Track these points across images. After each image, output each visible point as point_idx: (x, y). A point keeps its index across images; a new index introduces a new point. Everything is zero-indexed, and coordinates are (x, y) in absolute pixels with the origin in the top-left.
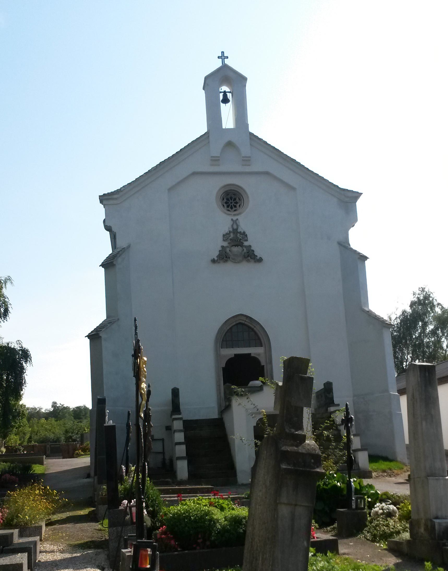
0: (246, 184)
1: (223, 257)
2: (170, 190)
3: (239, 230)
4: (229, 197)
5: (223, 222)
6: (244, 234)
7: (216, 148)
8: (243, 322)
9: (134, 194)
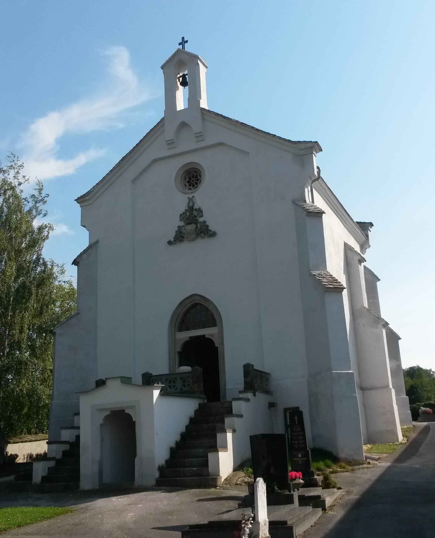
0: (202, 160)
1: (179, 237)
2: (134, 181)
4: (191, 175)
5: (180, 202)
6: (200, 211)
7: (170, 132)
8: (199, 302)
9: (103, 192)
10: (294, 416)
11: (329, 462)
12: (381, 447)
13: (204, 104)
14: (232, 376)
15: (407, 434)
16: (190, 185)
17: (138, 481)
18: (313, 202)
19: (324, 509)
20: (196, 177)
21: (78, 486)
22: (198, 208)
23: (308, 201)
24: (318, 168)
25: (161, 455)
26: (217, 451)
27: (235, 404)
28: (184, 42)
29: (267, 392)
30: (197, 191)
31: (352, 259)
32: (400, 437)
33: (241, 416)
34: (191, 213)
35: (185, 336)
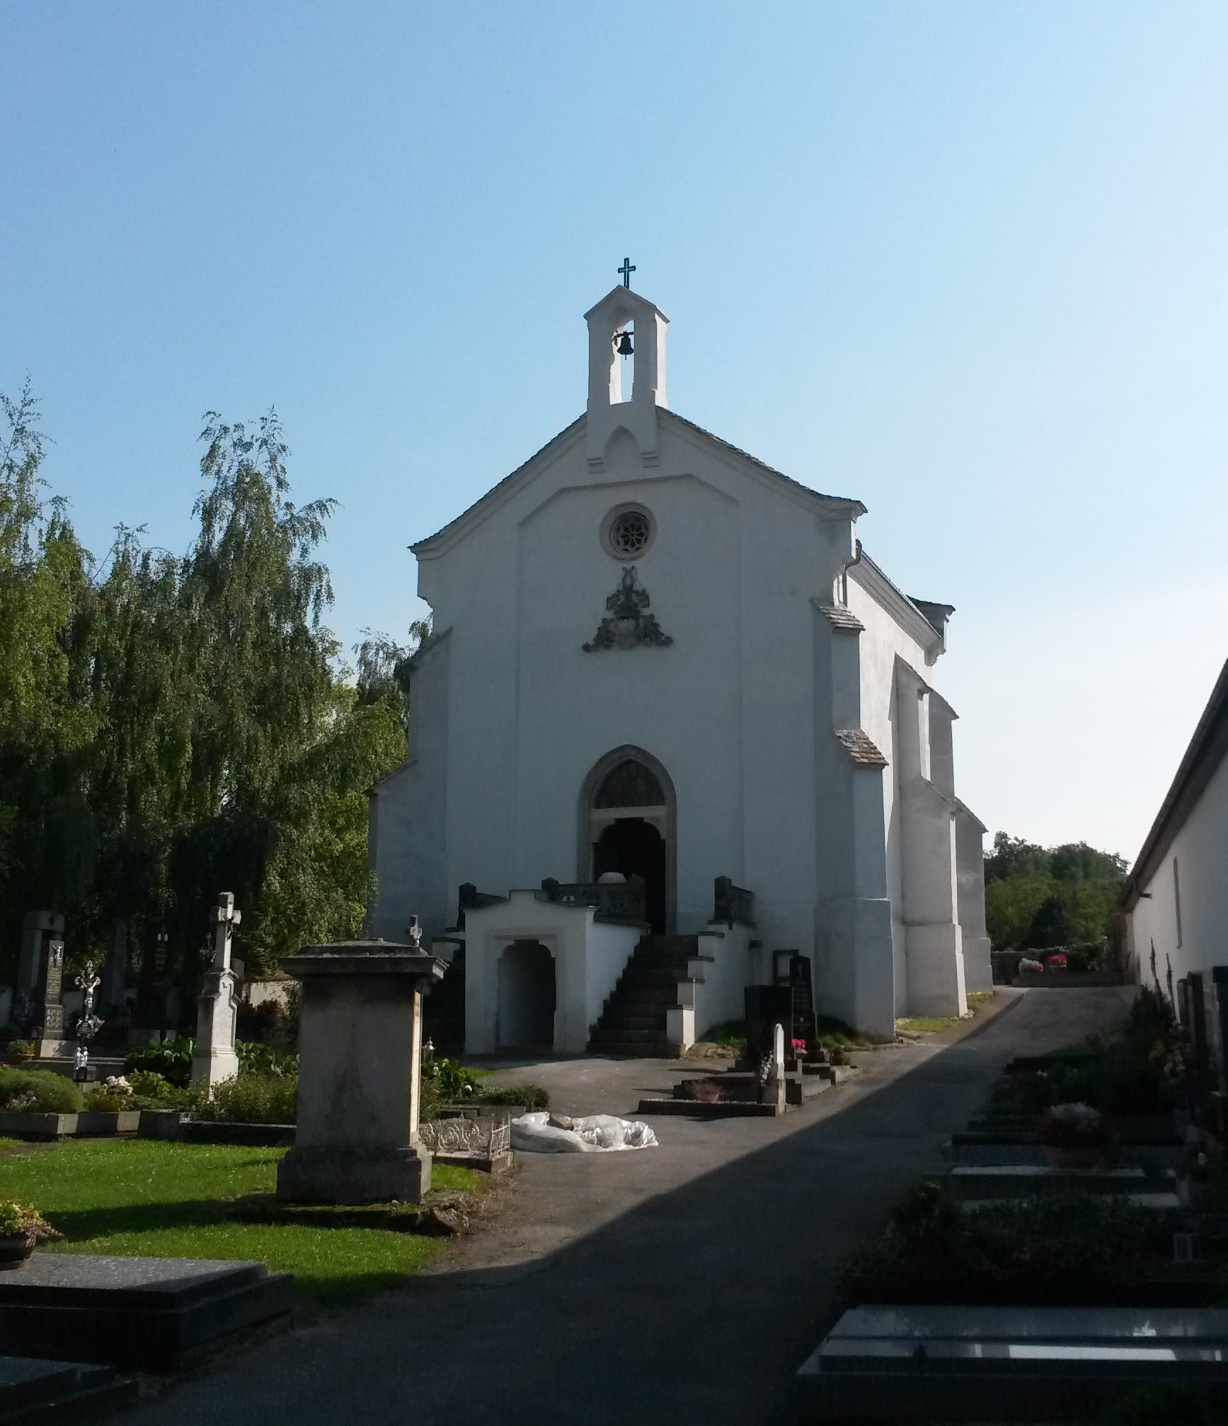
0: (655, 502)
1: (604, 639)
2: (522, 524)
3: (635, 588)
5: (607, 575)
6: (644, 595)
7: (595, 444)
10: (800, 964)
11: (841, 1037)
12: (926, 1022)
13: (661, 400)
14: (691, 893)
15: (977, 1005)
16: (626, 543)
17: (557, 1047)
18: (845, 603)
19: (833, 1082)
20: (639, 528)
21: (462, 1049)
22: (640, 589)
23: (836, 603)
24: (858, 541)
25: (593, 1011)
26: (681, 1008)
27: (703, 942)
28: (627, 269)
29: (748, 923)
30: (639, 557)
31: (906, 684)
32: (963, 1009)
33: (712, 960)
34: (629, 599)
35: (610, 815)
